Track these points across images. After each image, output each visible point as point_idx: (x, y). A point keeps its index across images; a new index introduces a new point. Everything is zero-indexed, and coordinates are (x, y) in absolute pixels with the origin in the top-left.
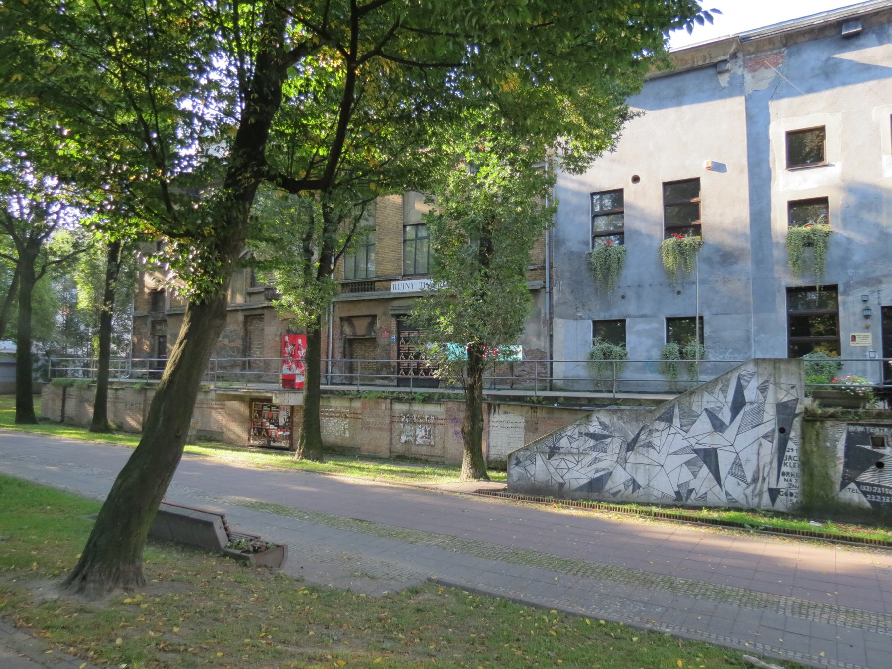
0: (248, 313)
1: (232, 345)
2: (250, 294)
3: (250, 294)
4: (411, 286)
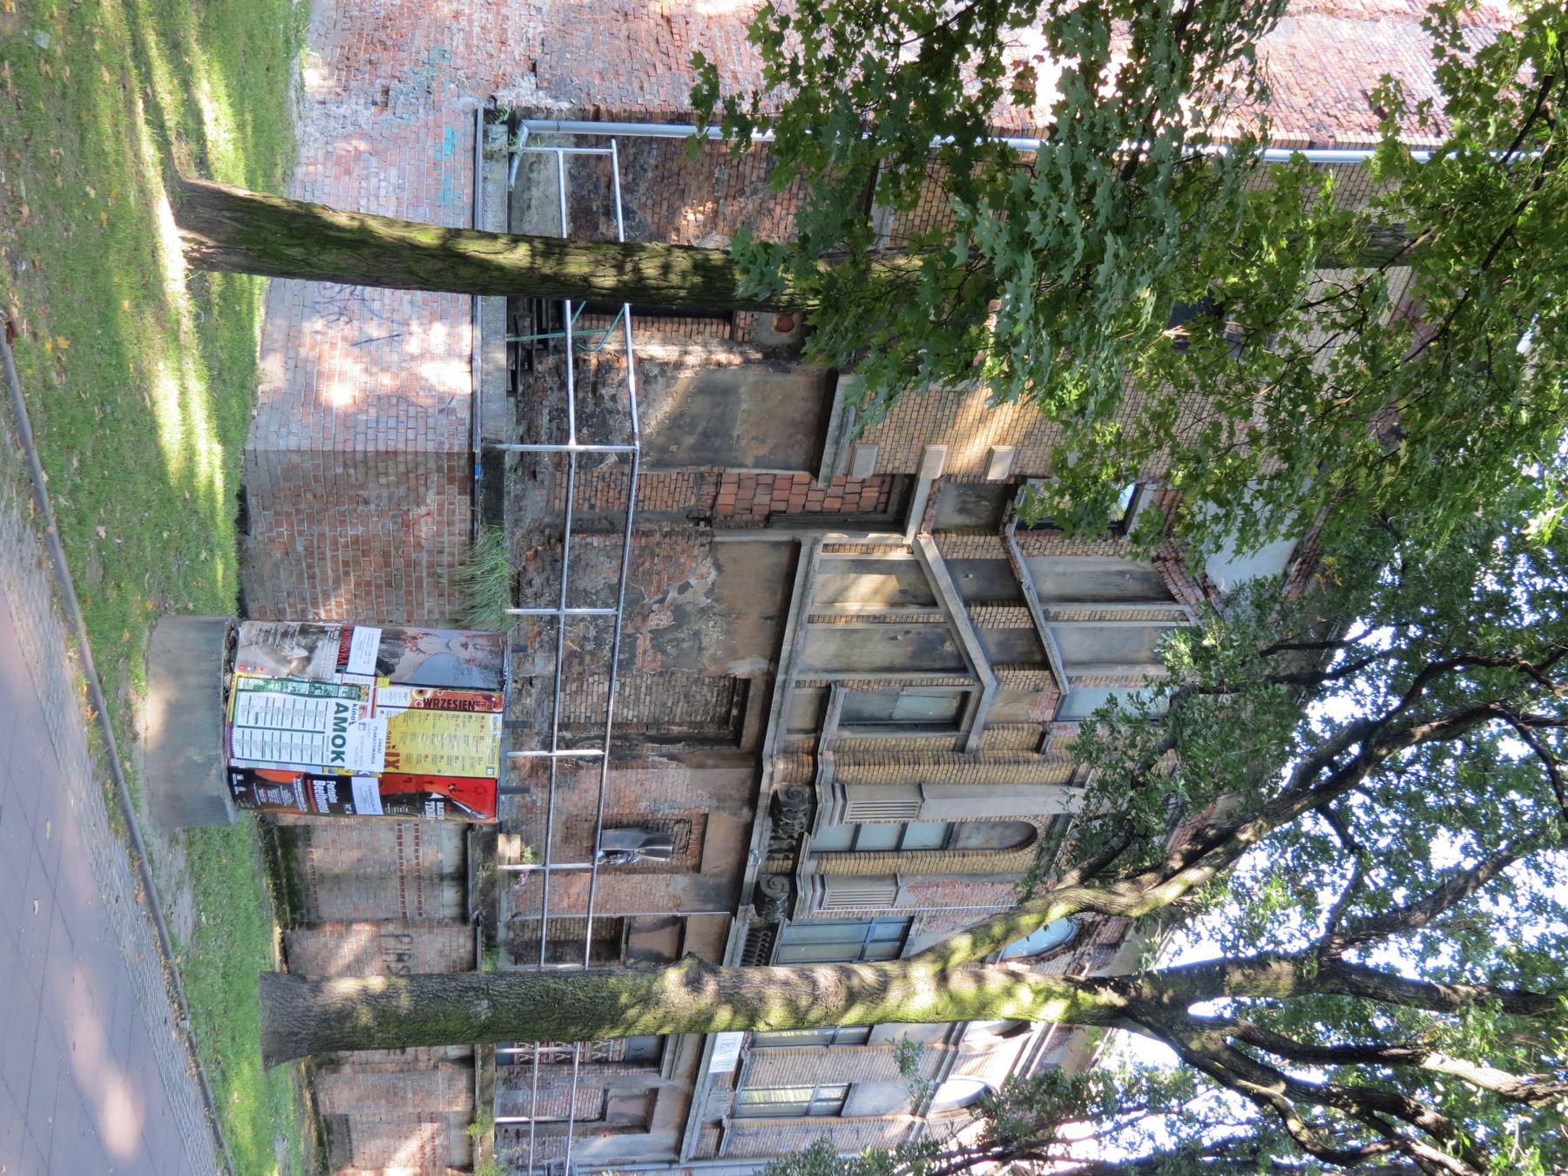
0: (755, 692)
1: (643, 643)
2: (824, 697)
3: (824, 697)
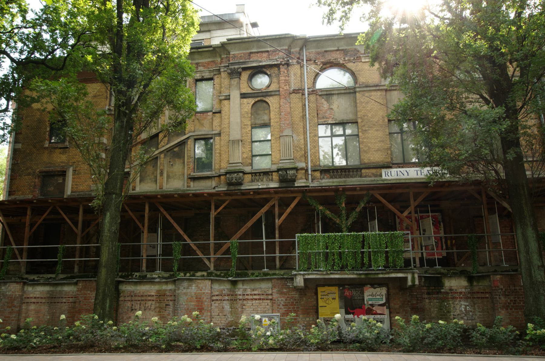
4: (406, 174)
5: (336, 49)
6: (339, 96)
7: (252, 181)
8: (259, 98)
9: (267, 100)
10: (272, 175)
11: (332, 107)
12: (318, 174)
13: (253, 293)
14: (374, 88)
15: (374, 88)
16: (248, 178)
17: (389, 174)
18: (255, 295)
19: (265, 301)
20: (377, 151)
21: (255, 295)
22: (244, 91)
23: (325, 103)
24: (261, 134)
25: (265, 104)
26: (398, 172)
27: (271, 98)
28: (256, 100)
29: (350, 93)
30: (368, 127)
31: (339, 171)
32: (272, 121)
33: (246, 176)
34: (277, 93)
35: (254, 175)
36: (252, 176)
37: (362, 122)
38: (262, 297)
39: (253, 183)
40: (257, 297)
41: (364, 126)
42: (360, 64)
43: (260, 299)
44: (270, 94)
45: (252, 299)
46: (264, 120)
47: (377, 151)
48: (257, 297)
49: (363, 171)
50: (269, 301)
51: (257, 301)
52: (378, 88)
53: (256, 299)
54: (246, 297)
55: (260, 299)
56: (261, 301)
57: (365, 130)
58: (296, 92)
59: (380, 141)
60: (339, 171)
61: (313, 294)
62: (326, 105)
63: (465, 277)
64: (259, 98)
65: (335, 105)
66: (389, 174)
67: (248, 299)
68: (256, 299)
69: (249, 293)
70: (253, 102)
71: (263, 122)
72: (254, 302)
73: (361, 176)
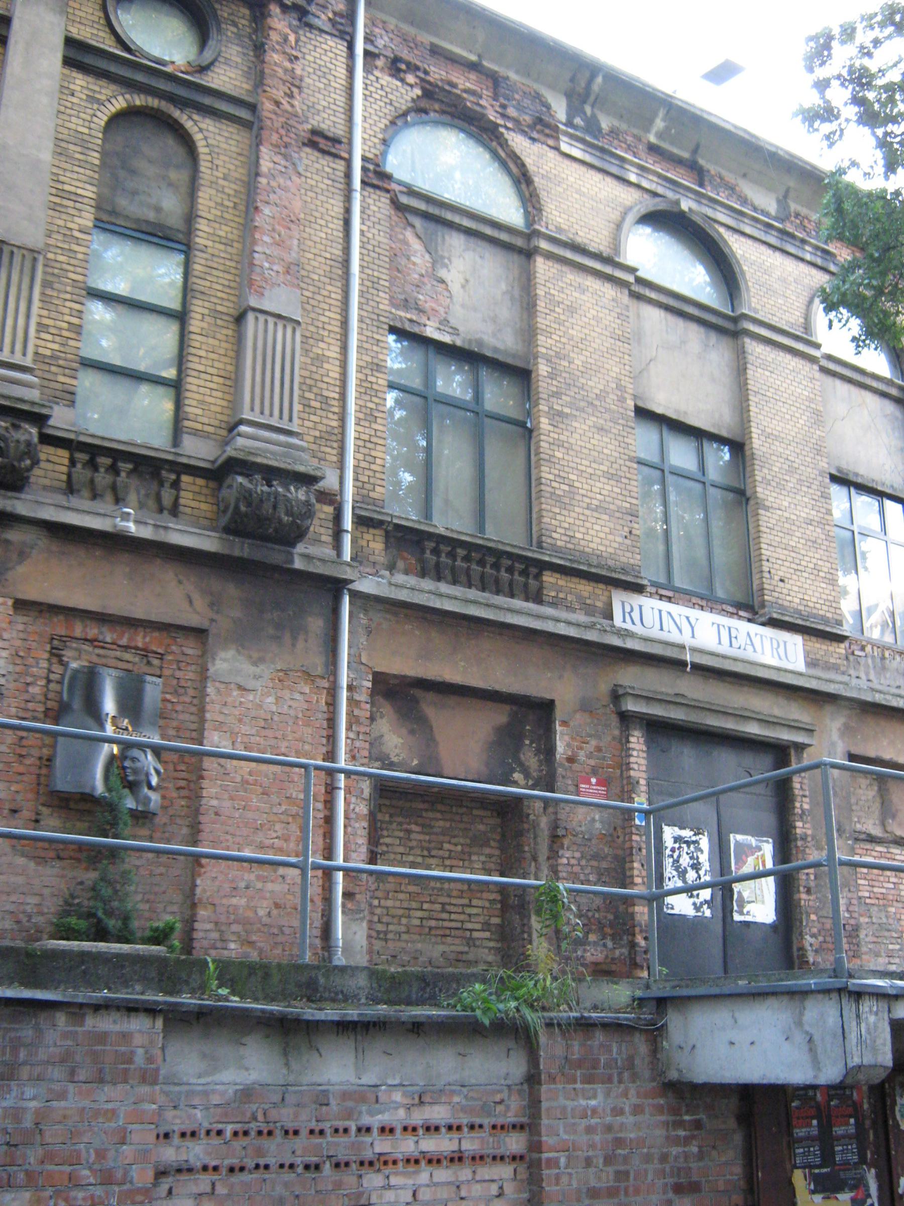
5: (473, 58)
6: (472, 241)
7: (70, 488)
8: (153, 102)
9: (188, 125)
10: (176, 485)
11: (442, 273)
12: (376, 544)
13: (418, 1117)
14: (598, 266)
15: (598, 266)
16: (53, 464)
17: (636, 615)
18: (431, 1129)
19: (486, 1172)
20: (597, 509)
21: (431, 1129)
22: (77, 32)
23: (416, 245)
24: (128, 268)
25: (170, 142)
26: (664, 615)
27: (208, 124)
28: (139, 100)
29: (508, 247)
30: (571, 405)
31: (461, 552)
32: (202, 225)
33: (46, 452)
34: (244, 114)
35: (82, 457)
36: (73, 462)
37: (552, 376)
38: (470, 1144)
39: (75, 501)
40: (443, 1144)
41: (557, 395)
42: (552, 154)
43: (457, 1158)
44: (207, 101)
45: (413, 1161)
46: (158, 209)
47: (597, 509)
48: (443, 1144)
49: (549, 578)
50: (505, 1171)
51: (443, 1174)
52: (608, 270)
53: (434, 1161)
54: (382, 1145)
55: (457, 1158)
56: (465, 1173)
57: (560, 414)
58: (323, 144)
59: (610, 476)
60: (461, 552)
61: (732, 1123)
62: (420, 259)
63: (529, 1071)
64: (153, 102)
65: (453, 271)
66: (636, 615)
67: (383, 1162)
68: (434, 1161)
69: (398, 1117)
70: (120, 103)
71: (151, 216)
72: (424, 1176)
73: (538, 599)
